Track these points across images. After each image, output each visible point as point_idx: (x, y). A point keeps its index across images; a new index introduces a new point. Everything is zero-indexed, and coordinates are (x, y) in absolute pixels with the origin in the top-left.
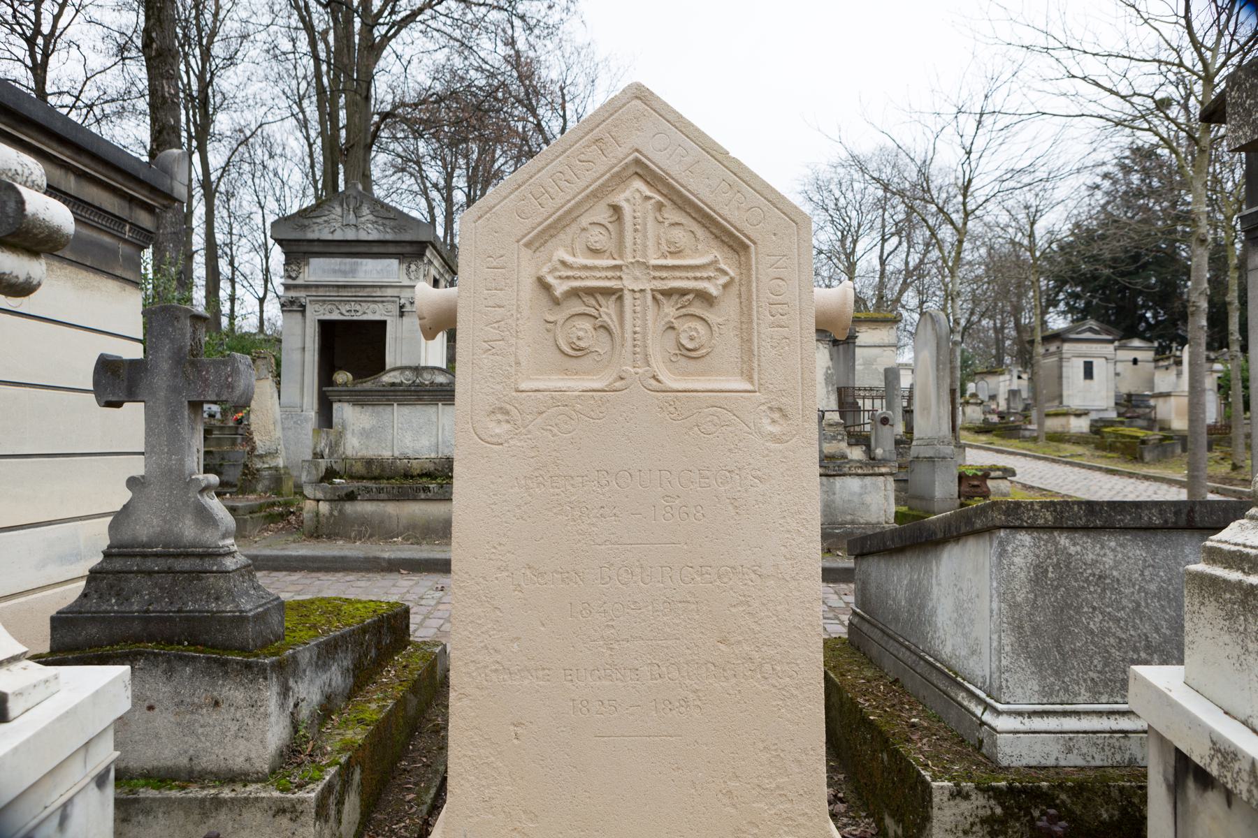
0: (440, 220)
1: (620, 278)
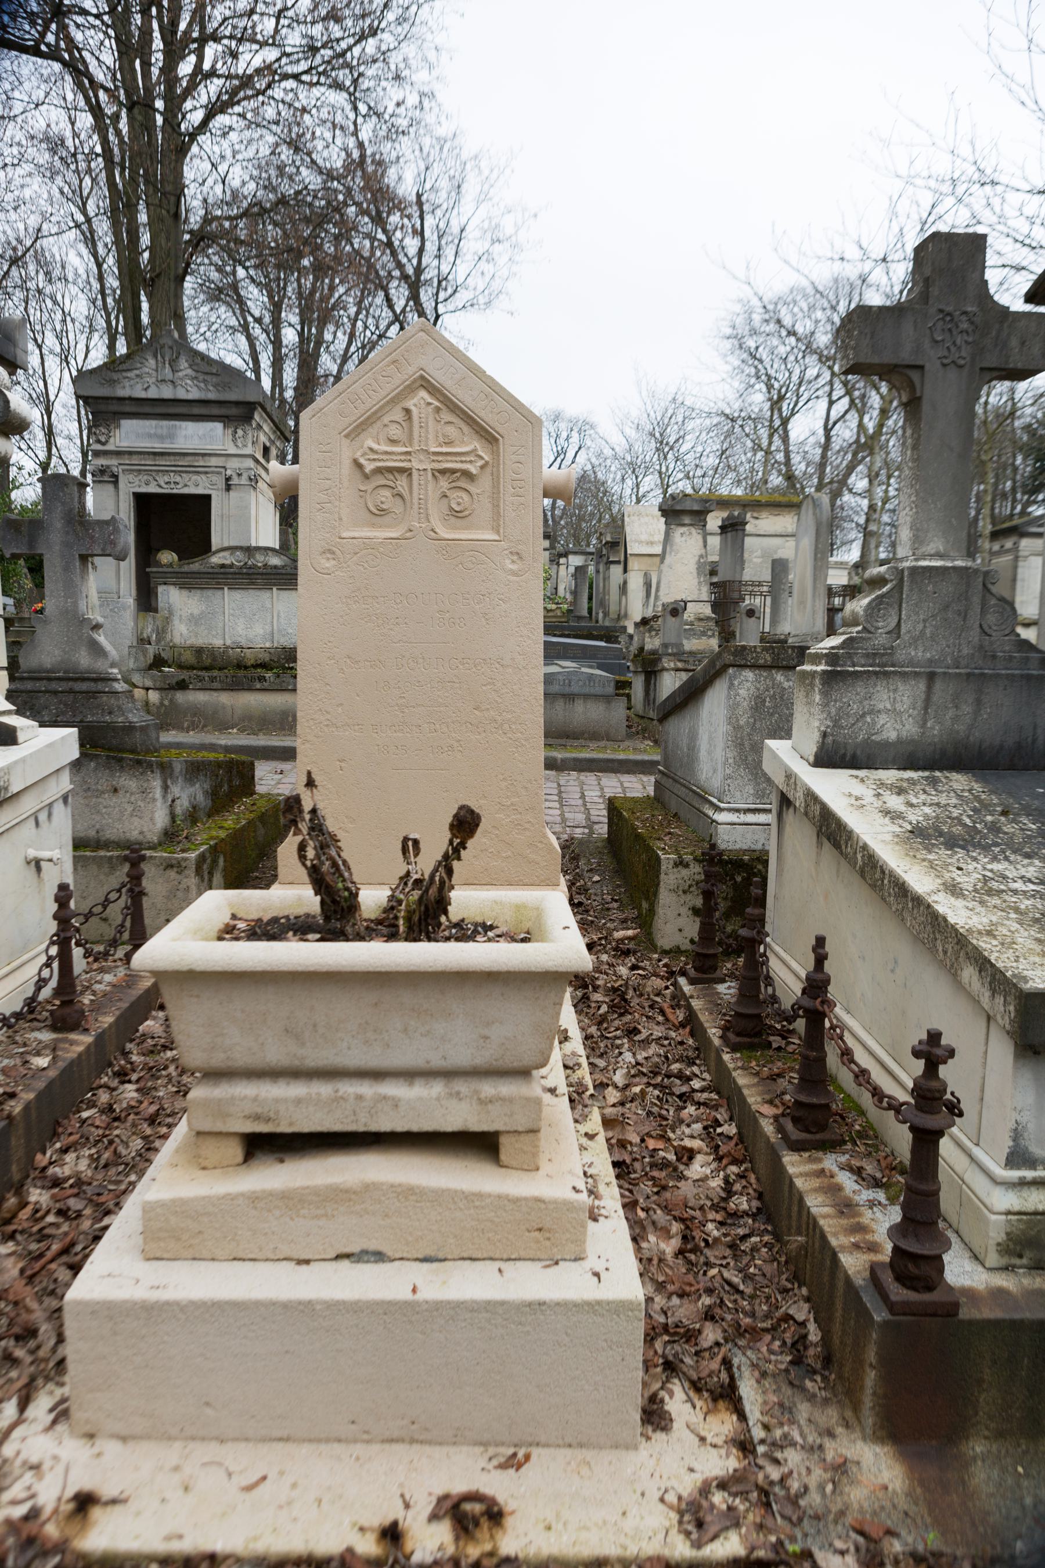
0: (265, 361)
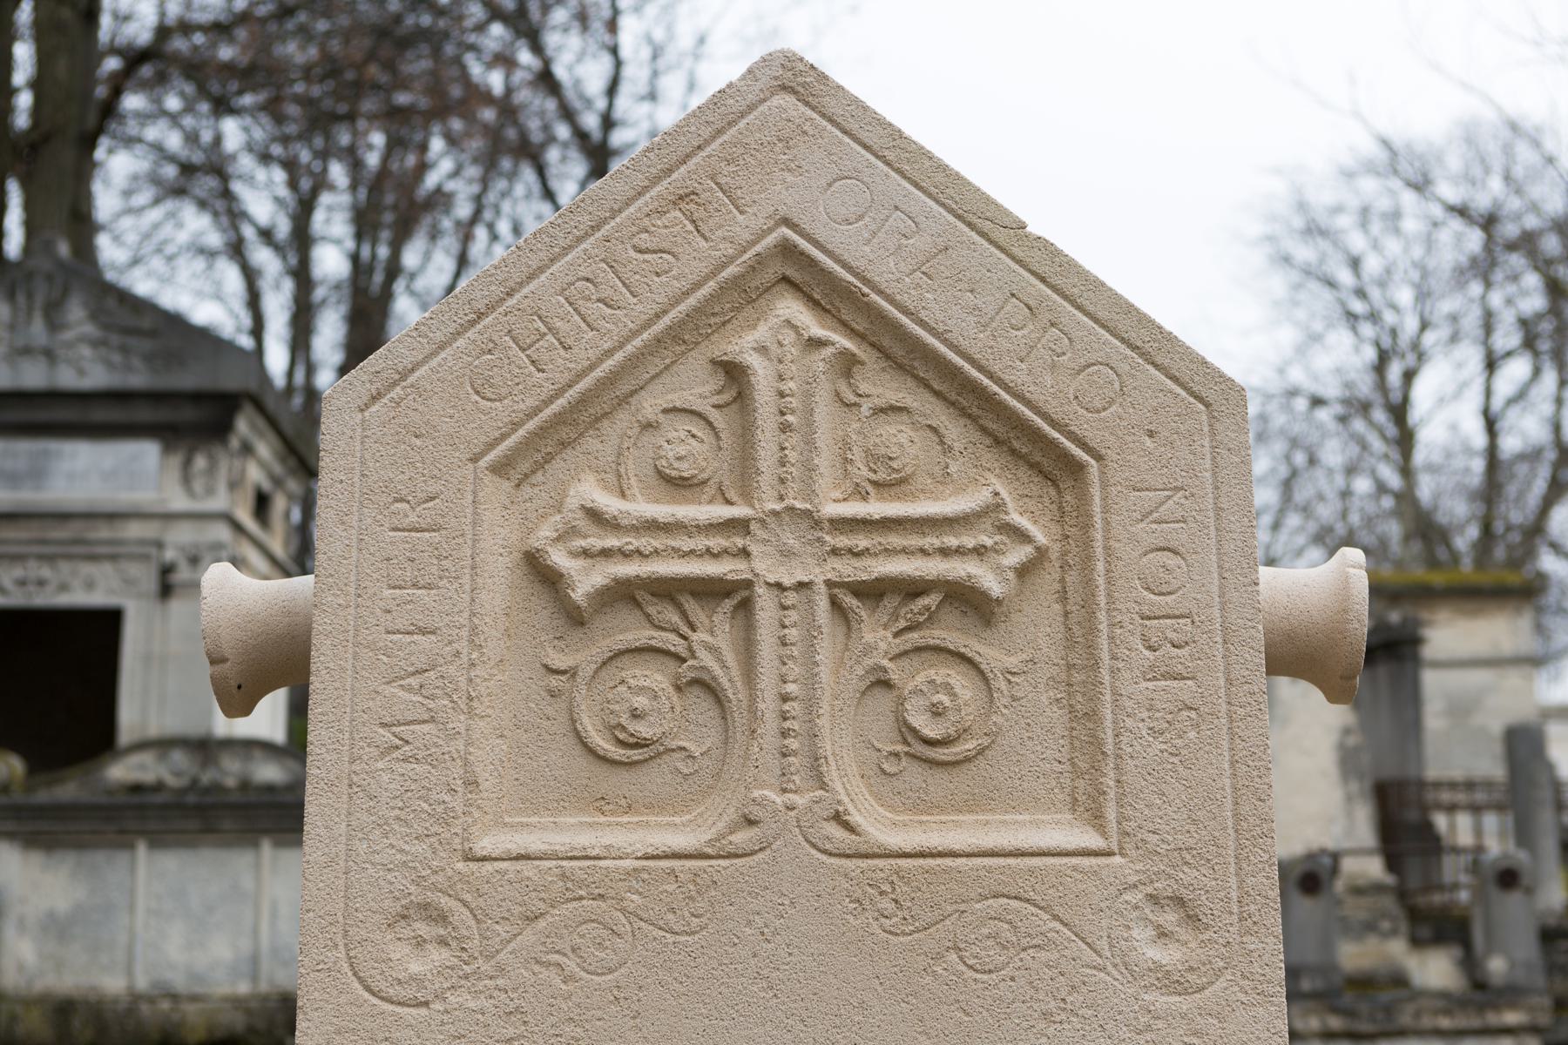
0: (277, 307)
1: (745, 553)
